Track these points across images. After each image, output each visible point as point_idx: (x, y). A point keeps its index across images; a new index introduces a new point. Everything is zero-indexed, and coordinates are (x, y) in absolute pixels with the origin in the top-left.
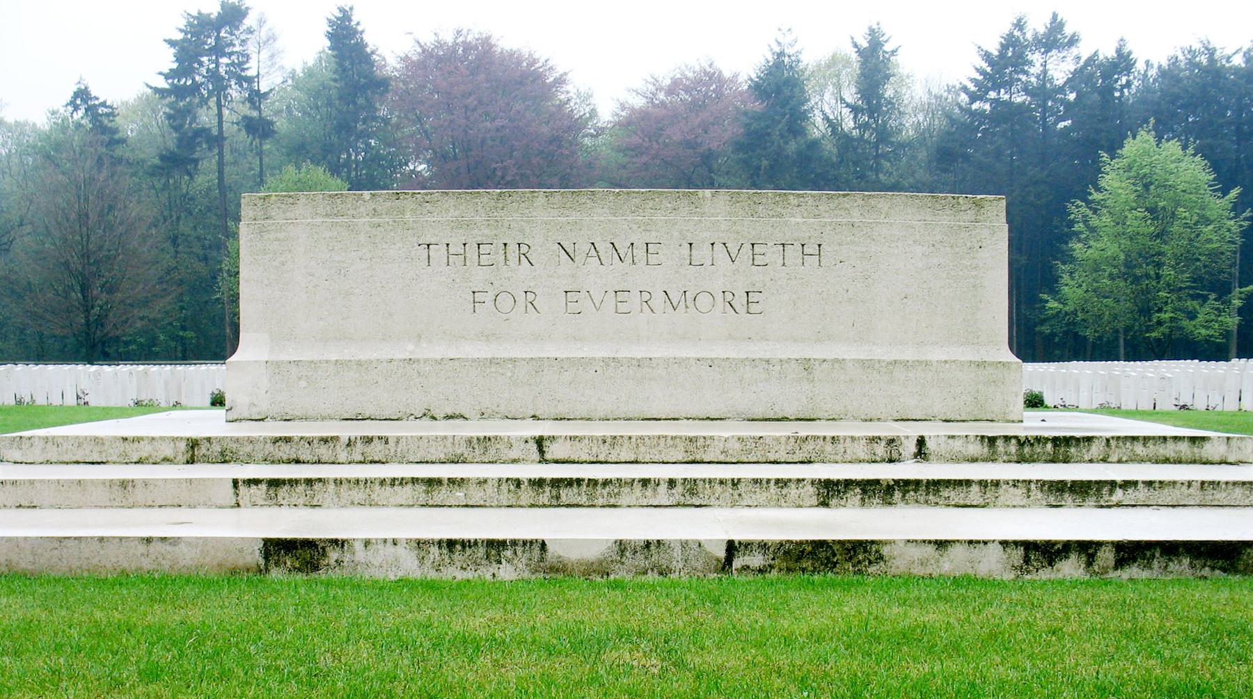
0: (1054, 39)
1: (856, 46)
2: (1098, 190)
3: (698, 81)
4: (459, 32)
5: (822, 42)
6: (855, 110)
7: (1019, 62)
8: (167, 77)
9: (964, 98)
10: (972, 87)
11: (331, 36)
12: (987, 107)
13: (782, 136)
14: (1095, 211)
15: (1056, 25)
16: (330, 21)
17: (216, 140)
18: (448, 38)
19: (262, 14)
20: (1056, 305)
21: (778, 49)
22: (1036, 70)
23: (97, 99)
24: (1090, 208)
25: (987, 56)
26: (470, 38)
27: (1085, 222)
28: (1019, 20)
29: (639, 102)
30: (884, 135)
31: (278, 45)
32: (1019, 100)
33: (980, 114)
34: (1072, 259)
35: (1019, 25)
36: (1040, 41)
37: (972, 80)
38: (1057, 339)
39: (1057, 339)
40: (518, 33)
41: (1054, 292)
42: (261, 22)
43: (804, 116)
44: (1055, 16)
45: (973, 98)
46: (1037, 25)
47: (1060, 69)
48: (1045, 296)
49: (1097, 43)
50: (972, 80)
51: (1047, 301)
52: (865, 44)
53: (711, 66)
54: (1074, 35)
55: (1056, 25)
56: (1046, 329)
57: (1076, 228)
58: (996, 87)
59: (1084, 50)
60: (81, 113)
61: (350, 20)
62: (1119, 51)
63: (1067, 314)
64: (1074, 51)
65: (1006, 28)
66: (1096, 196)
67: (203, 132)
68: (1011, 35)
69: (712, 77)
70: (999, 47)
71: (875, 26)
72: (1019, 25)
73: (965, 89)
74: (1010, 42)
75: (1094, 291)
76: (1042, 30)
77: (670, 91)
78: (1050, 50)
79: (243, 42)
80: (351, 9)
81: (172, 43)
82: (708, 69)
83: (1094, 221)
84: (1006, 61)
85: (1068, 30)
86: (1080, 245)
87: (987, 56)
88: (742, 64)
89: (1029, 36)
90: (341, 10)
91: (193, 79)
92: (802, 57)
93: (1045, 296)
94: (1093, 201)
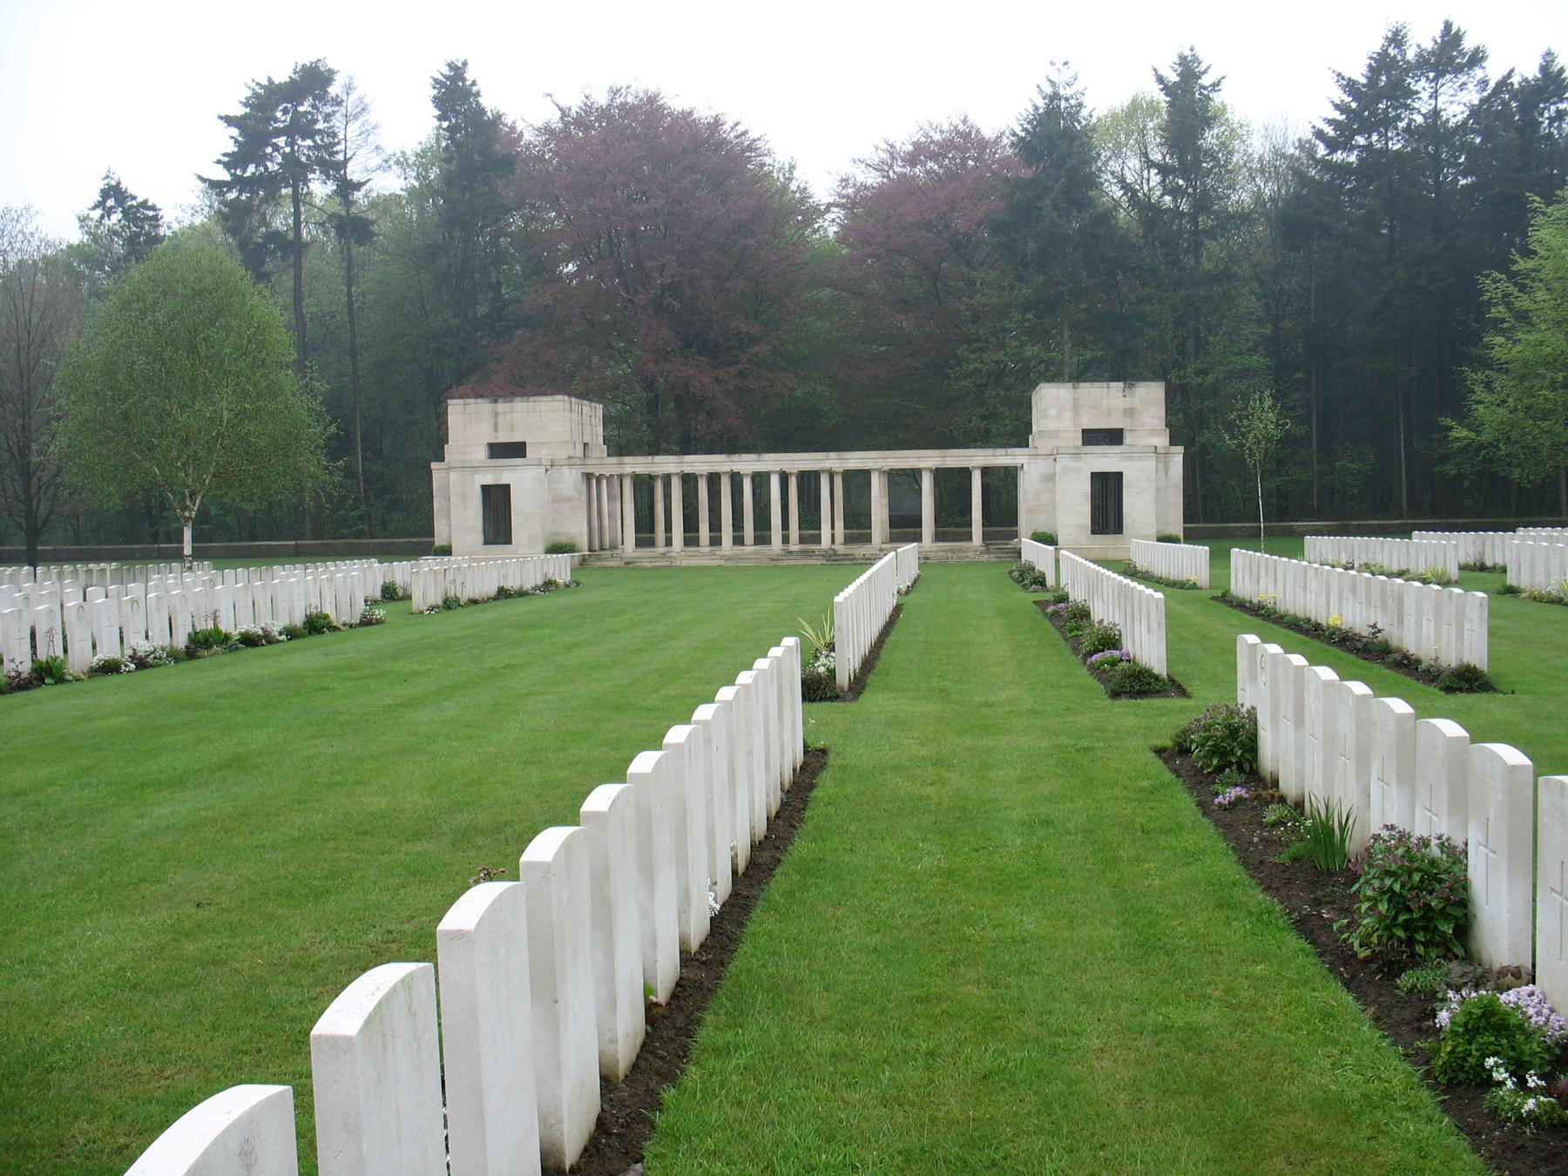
0: (1450, 56)
1: (1160, 80)
2: (1528, 253)
3: (947, 145)
4: (615, 92)
5: (1114, 83)
6: (1164, 170)
7: (1401, 94)
8: (227, 166)
9: (1321, 150)
10: (1330, 131)
11: (439, 102)
12: (1353, 158)
13: (1055, 207)
14: (1523, 288)
15: (1451, 38)
16: (436, 80)
17: (291, 247)
18: (602, 99)
19: (351, 78)
20: (1465, 433)
21: (1049, 90)
22: (1424, 104)
23: (134, 198)
24: (1515, 284)
25: (1350, 86)
26: (630, 99)
27: (1508, 305)
28: (1396, 33)
29: (873, 179)
30: (1203, 203)
31: (371, 118)
32: (1396, 147)
33: (1344, 168)
34: (1485, 363)
35: (1397, 39)
36: (1427, 61)
37: (1330, 122)
38: (1467, 483)
39: (1467, 483)
40: (699, 85)
41: (1462, 415)
42: (349, 89)
43: (1092, 182)
44: (1448, 26)
45: (1333, 146)
46: (1423, 38)
47: (1455, 101)
48: (1448, 421)
49: (1512, 57)
50: (1330, 122)
51: (1450, 429)
52: (1173, 78)
53: (965, 122)
54: (1477, 50)
55: (1451, 38)
56: (1450, 469)
57: (1494, 313)
58: (1367, 130)
59: (1493, 71)
60: (115, 217)
61: (464, 80)
62: (1544, 69)
63: (1482, 446)
64: (1478, 73)
65: (1376, 45)
66: (1523, 264)
67: (275, 236)
68: (1384, 54)
69: (965, 141)
70: (1365, 70)
71: (1187, 53)
72: (1397, 39)
73: (1319, 134)
74: (1381, 63)
75: (1529, 408)
76: (1429, 45)
77: (912, 159)
78: (1443, 76)
79: (328, 117)
80: (465, 64)
81: (229, 121)
82: (961, 128)
83: (1523, 302)
84: (1382, 87)
85: (1468, 44)
86: (1500, 340)
87: (1350, 86)
88: (1002, 116)
89: (1411, 55)
90: (451, 66)
91: (266, 168)
92: (1086, 100)
93: (1448, 421)
94: (1517, 273)
